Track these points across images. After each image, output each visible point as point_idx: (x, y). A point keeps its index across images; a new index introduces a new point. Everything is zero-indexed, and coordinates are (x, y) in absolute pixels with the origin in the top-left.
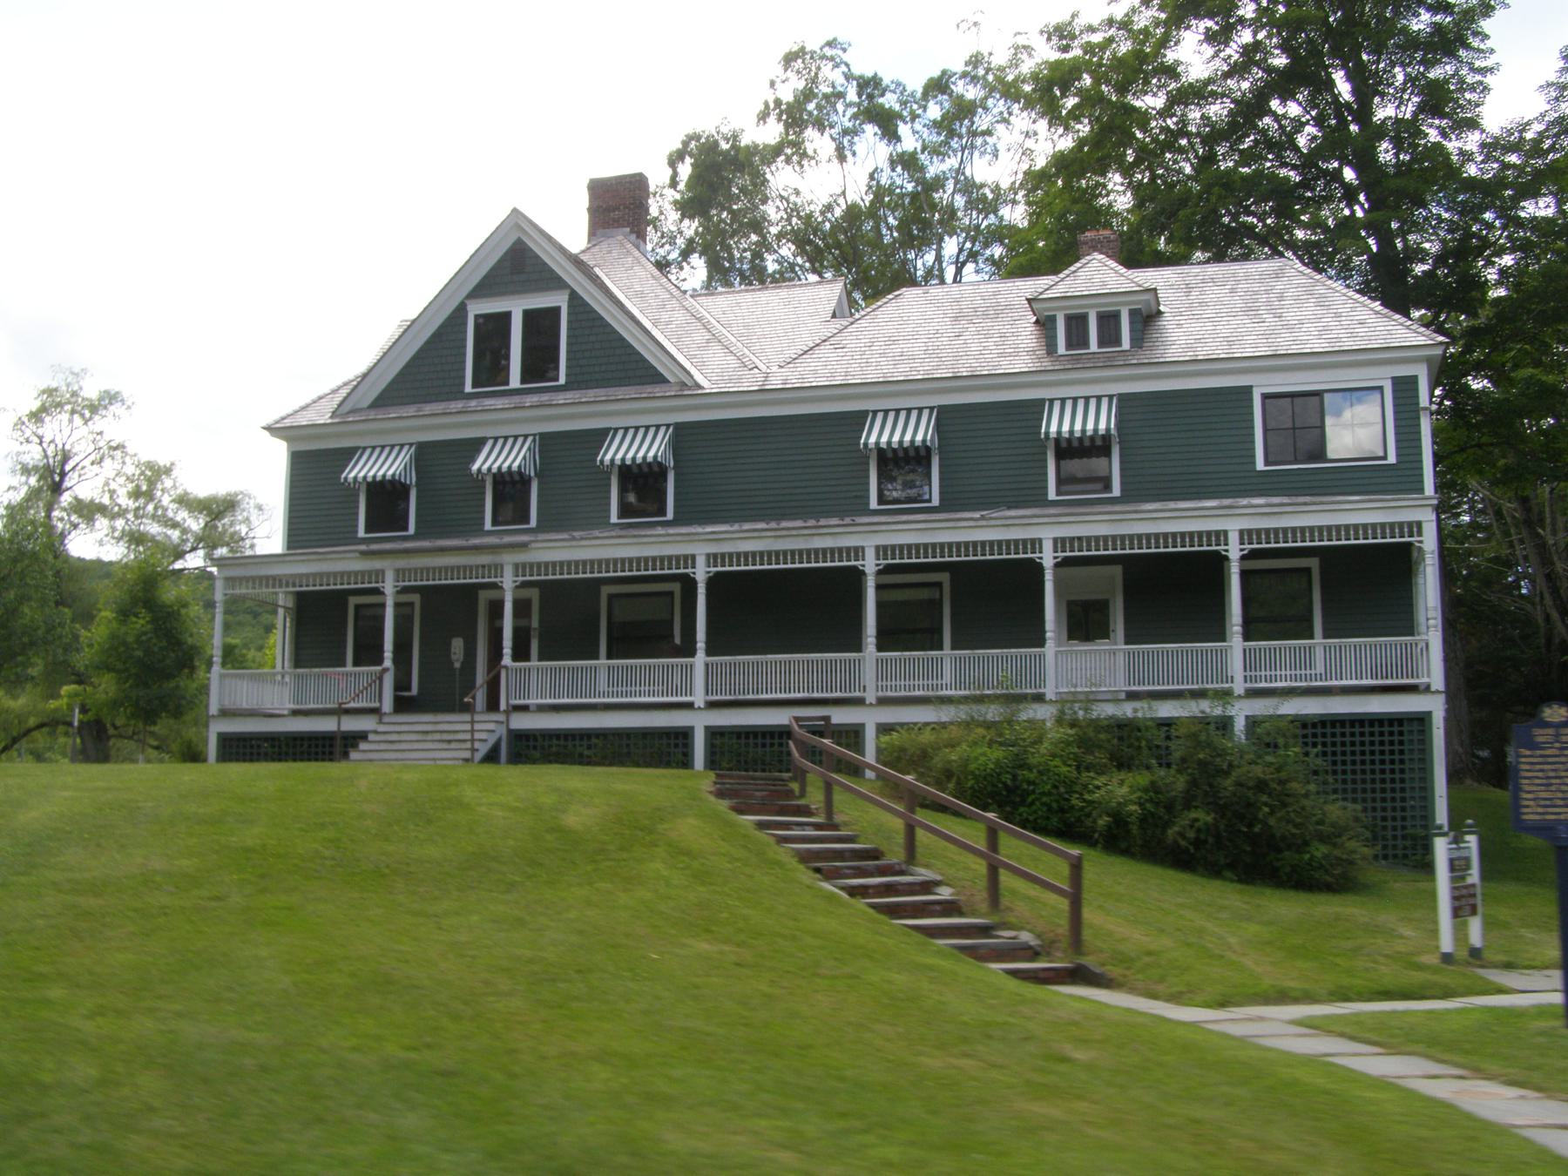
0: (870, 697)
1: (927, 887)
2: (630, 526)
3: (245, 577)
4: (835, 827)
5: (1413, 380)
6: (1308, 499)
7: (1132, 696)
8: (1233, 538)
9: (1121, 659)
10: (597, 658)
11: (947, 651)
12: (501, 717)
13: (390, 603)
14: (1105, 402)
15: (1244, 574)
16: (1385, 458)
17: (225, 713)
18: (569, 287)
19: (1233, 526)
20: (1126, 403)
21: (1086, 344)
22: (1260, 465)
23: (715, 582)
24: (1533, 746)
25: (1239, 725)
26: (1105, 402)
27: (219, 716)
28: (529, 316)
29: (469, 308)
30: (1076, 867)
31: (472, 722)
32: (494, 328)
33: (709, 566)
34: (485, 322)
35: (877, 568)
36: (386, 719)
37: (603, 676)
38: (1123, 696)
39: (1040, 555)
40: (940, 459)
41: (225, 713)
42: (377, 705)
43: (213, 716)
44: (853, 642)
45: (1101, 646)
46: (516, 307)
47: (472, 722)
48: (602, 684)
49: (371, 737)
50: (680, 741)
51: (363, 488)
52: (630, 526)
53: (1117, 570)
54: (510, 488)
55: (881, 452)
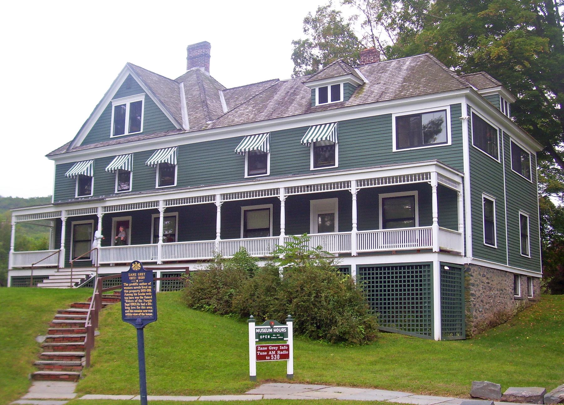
0: (354, 253)
2: (162, 189)
3: (29, 215)
5: (459, 105)
6: (358, 169)
10: (240, 238)
11: (417, 227)
12: (95, 269)
13: (162, 216)
16: (447, 143)
17: (15, 269)
18: (145, 92)
22: (394, 149)
23: (289, 200)
27: (438, 253)
28: (132, 104)
29: (113, 104)
31: (72, 272)
32: (120, 110)
33: (358, 186)
34: (118, 108)
35: (221, 204)
36: (60, 270)
37: (381, 237)
38: (337, 255)
39: (430, 180)
40: (271, 155)
41: (15, 269)
42: (56, 265)
43: (10, 270)
44: (214, 237)
46: (127, 102)
47: (72, 272)
48: (381, 243)
49: (50, 278)
50: (426, 269)
51: (78, 178)
52: (162, 189)
53: (336, 200)
54: (123, 176)
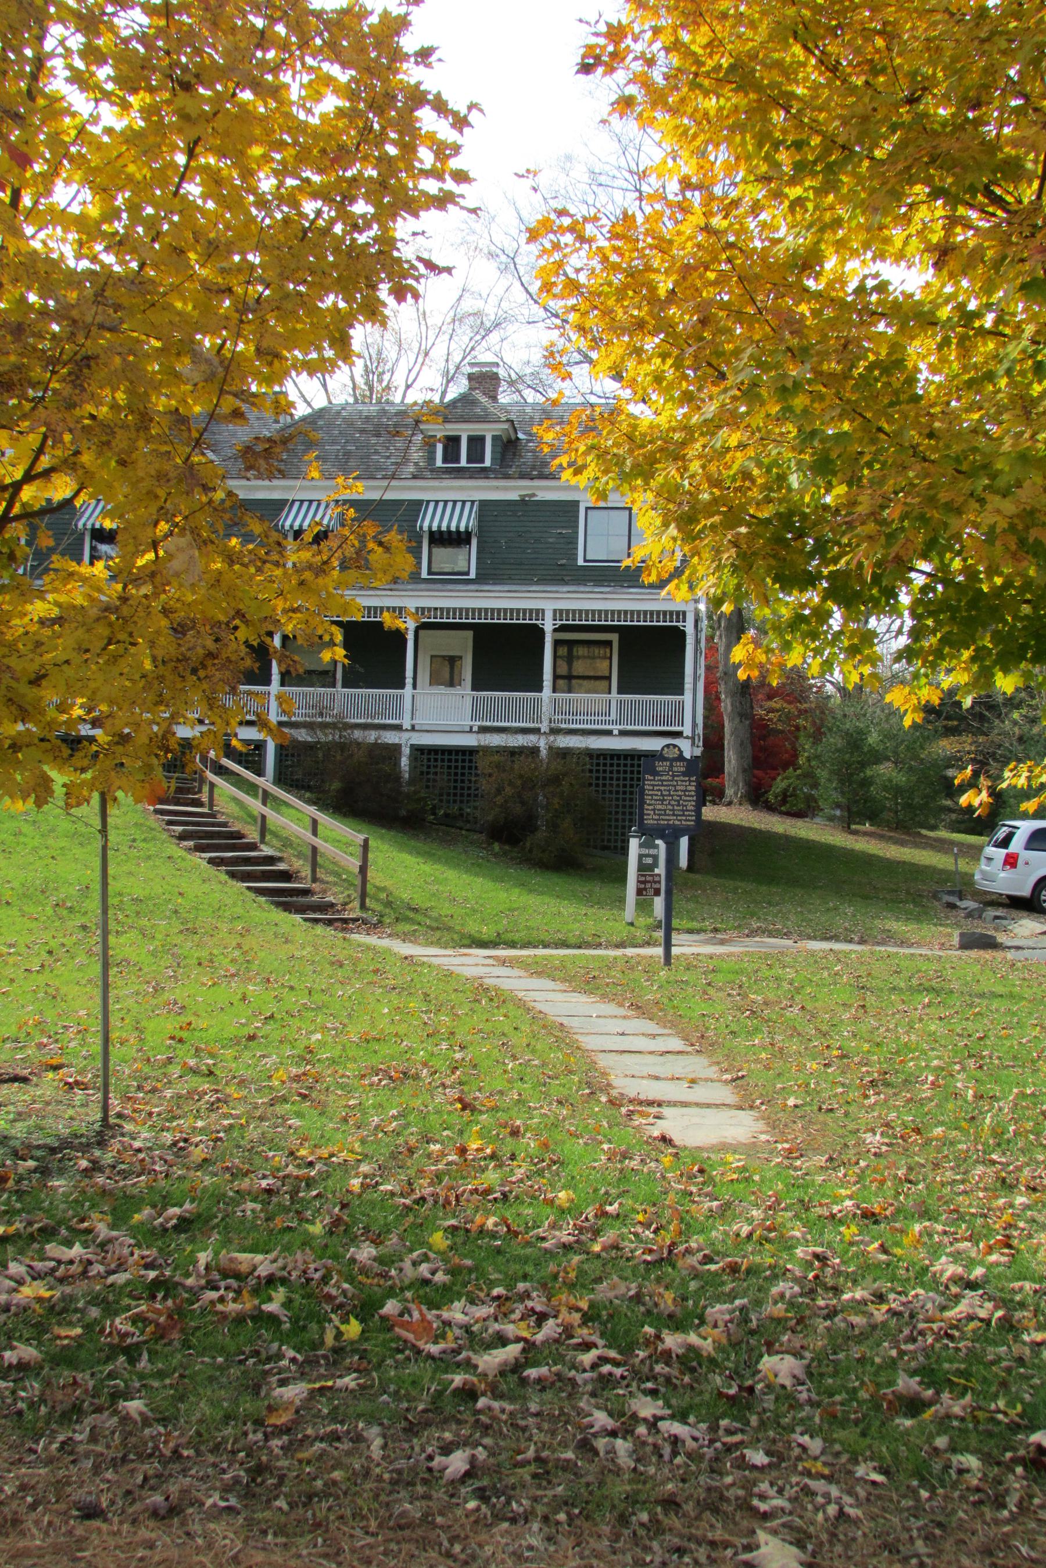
1: (271, 860)
4: (214, 816)
7: (483, 730)
8: (549, 615)
9: (468, 701)
14: (468, 505)
15: (557, 643)
19: (549, 606)
20: (485, 507)
21: (457, 460)
24: (655, 773)
25: (544, 753)
26: (468, 505)
30: (365, 846)
45: (457, 690)
55: (431, 533)
